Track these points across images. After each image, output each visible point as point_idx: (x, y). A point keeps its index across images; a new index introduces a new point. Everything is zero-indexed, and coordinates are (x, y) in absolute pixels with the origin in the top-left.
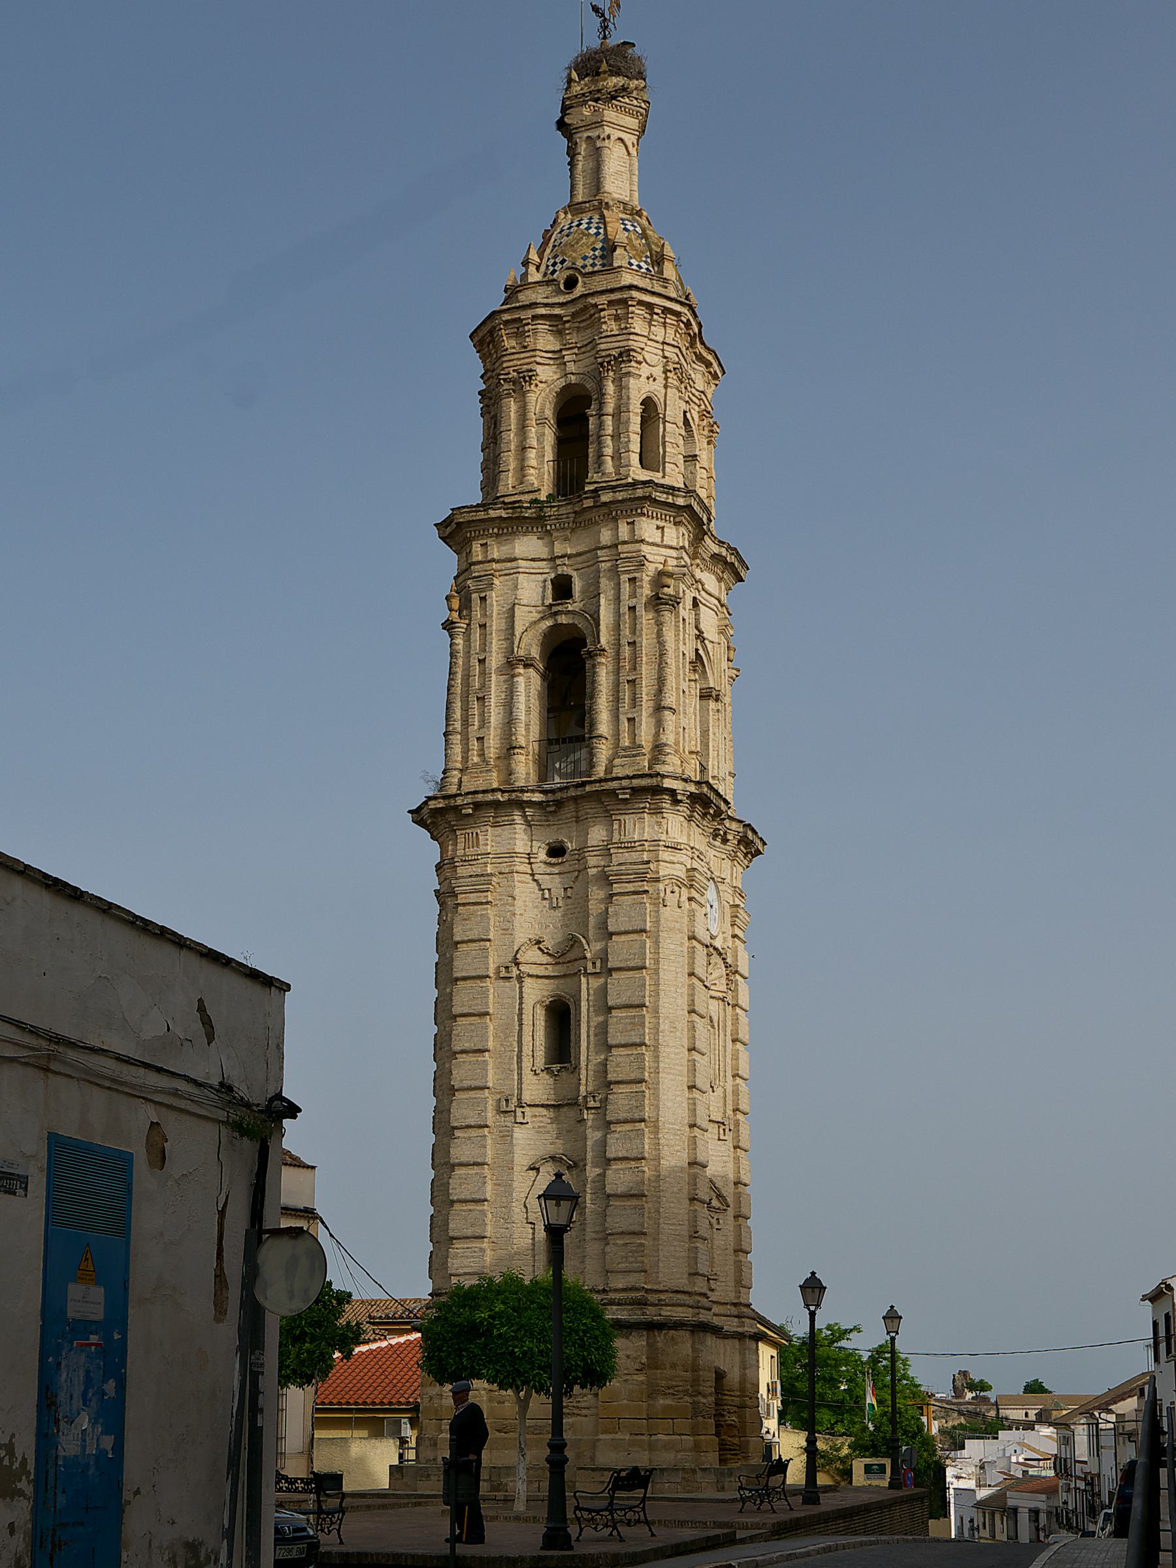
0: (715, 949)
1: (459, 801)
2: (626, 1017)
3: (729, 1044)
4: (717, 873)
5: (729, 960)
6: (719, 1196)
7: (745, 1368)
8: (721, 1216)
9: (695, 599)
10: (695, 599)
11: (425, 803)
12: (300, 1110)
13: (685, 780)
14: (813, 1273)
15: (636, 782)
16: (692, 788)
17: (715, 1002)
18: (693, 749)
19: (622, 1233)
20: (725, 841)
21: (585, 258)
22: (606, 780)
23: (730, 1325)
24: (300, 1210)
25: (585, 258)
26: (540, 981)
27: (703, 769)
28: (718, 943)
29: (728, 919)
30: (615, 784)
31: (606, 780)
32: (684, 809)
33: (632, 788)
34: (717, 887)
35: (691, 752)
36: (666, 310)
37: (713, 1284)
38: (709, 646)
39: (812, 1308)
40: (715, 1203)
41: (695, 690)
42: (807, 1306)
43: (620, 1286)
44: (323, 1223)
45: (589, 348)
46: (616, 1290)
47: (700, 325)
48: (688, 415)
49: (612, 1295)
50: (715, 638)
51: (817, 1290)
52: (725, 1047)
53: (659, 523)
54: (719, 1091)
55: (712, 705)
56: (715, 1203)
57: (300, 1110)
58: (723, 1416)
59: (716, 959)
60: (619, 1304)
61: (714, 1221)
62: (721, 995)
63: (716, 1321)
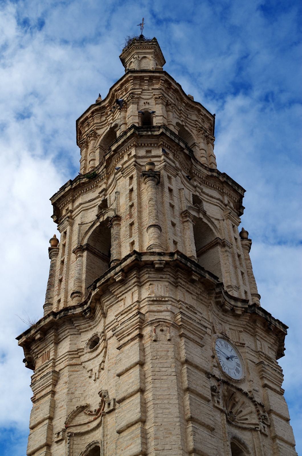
9: (195, 197)
16: (167, 258)
38: (216, 222)
62: (253, 427)
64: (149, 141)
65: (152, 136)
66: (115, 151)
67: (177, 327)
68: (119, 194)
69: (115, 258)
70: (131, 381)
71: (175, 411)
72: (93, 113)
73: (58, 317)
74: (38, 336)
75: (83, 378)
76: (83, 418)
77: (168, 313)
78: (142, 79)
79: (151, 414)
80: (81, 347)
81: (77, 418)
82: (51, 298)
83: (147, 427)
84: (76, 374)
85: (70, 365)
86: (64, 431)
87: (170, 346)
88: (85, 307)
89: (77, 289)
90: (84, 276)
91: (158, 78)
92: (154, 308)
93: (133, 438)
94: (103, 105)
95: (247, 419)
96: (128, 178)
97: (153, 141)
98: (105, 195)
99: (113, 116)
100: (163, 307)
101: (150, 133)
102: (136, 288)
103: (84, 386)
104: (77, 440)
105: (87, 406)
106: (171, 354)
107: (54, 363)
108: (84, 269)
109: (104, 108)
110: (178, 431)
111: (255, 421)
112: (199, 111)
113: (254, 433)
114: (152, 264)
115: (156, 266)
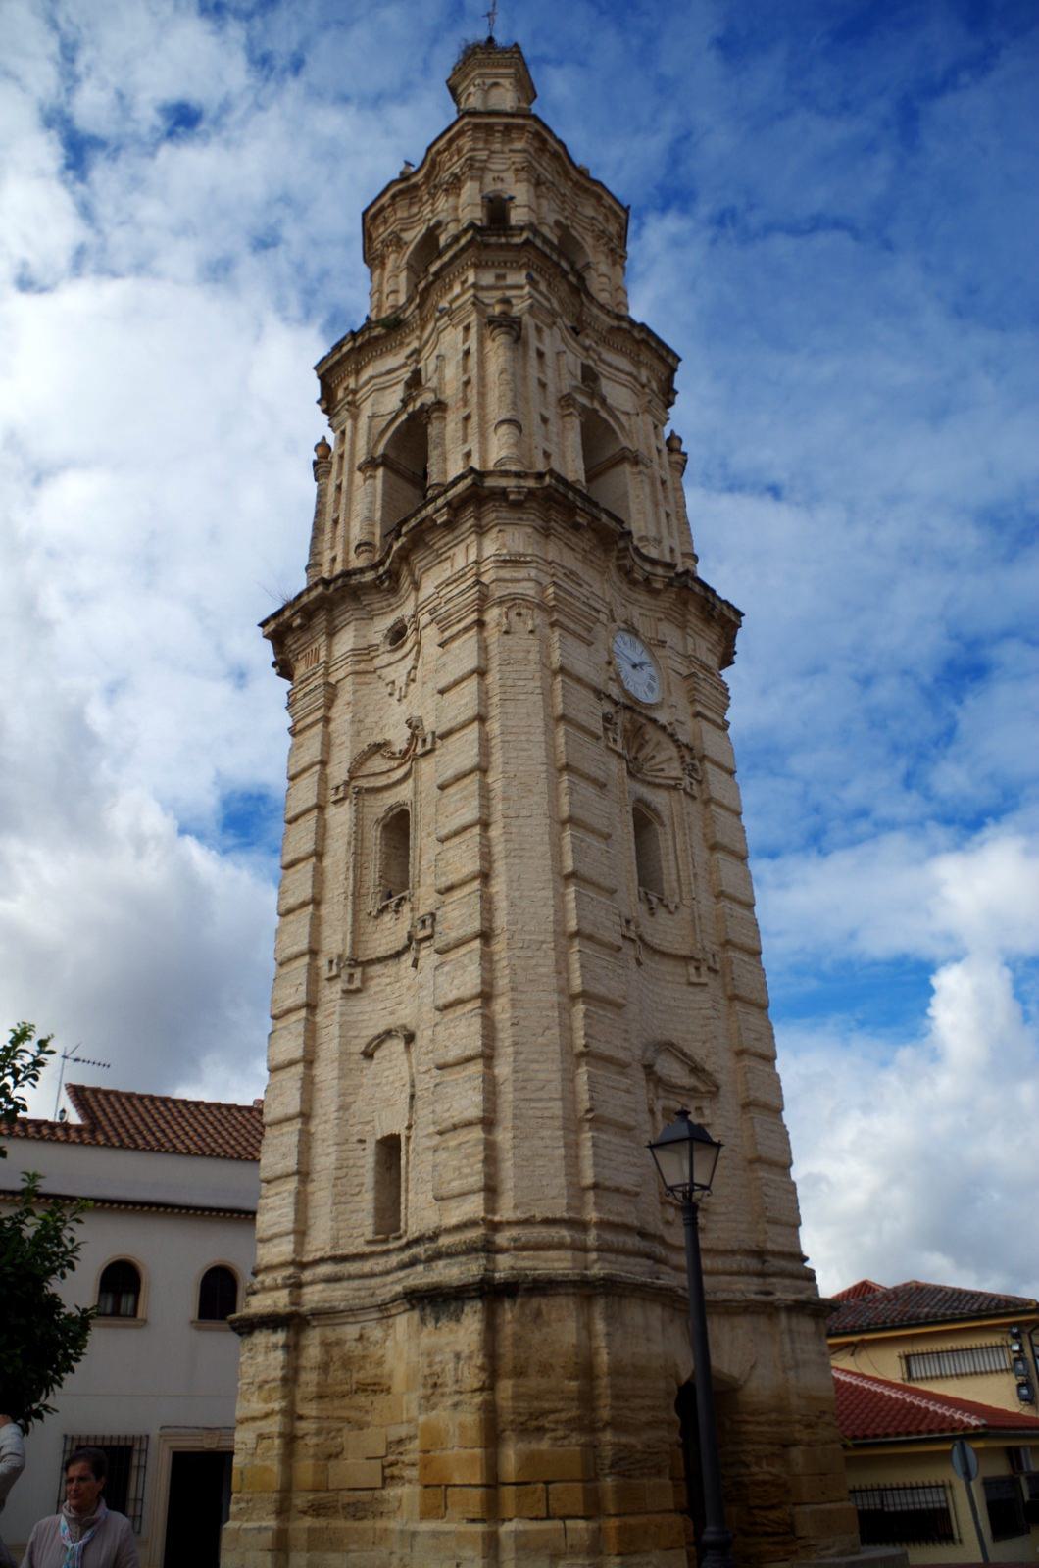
16: (531, 483)
38: (623, 418)
62: (673, 783)
64: (502, 256)
65: (509, 247)
66: (437, 274)
67: (542, 606)
70: (463, 702)
71: (539, 753)
72: (394, 197)
76: (379, 764)
77: (531, 584)
78: (489, 129)
83: (490, 780)
84: (365, 690)
85: (356, 673)
86: (347, 784)
90: (378, 515)
91: (521, 128)
92: (505, 574)
93: (465, 798)
94: (413, 180)
95: (662, 770)
96: (460, 328)
97: (510, 255)
98: (417, 361)
99: (433, 204)
100: (522, 574)
103: (381, 709)
105: (386, 744)
106: (534, 656)
109: (416, 187)
113: (674, 793)
114: (503, 493)
115: (512, 497)
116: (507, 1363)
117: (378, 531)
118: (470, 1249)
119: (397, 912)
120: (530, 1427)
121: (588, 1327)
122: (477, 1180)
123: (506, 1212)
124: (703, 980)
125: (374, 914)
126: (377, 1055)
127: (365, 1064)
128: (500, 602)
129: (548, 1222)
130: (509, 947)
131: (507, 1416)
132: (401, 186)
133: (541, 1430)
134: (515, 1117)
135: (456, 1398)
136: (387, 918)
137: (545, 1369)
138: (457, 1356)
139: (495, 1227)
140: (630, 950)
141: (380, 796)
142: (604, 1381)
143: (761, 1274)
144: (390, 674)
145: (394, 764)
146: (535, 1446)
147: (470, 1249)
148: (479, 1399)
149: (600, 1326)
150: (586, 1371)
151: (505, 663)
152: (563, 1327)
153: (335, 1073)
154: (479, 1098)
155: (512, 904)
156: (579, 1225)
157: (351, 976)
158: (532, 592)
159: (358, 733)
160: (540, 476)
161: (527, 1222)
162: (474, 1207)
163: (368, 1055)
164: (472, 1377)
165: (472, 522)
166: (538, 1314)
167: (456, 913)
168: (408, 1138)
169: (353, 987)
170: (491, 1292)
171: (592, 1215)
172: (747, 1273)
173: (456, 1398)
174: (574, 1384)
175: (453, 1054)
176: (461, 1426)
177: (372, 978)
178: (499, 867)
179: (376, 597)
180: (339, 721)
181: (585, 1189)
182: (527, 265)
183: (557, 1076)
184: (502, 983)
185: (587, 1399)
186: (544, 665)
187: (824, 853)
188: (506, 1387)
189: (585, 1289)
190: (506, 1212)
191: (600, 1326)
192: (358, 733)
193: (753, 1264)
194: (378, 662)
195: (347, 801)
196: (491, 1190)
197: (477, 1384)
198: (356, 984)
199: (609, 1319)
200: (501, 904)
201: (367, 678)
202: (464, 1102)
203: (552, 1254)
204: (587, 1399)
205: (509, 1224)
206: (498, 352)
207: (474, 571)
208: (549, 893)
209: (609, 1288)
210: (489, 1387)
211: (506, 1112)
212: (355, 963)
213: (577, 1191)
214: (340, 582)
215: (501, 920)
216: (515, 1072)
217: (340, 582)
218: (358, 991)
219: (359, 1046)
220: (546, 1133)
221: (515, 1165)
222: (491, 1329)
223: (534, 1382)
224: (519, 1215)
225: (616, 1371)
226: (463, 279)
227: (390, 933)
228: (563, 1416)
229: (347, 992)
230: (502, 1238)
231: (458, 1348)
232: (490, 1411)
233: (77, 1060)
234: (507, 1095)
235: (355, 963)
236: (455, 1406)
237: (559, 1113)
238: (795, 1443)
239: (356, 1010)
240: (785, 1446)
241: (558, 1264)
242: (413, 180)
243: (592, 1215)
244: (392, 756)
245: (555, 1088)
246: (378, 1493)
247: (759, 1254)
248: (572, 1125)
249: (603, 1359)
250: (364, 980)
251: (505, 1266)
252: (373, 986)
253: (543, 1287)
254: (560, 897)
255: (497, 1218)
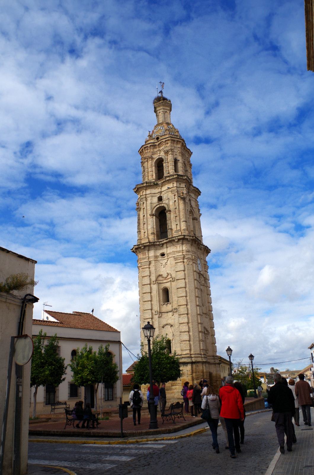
0: (201, 274)
1: (141, 246)
2: (181, 290)
3: (206, 296)
4: (200, 257)
5: (205, 276)
6: (207, 331)
7: (217, 371)
8: (208, 335)
9: (190, 199)
10: (190, 199)
11: (134, 247)
12: (39, 299)
13: (190, 236)
14: (229, 347)
15: (179, 237)
16: (191, 238)
17: (202, 286)
18: (192, 230)
19: (184, 341)
20: (201, 249)
21: (160, 133)
22: (172, 238)
23: (212, 361)
24: (117, 342)
25: (160, 133)
26: (285, 361)
27: (195, 234)
28: (202, 273)
29: (203, 267)
30: (174, 238)
31: (172, 238)
32: (190, 243)
33: (178, 239)
34: (200, 260)
35: (191, 231)
36: (178, 141)
37: (207, 352)
38: (194, 209)
39: (230, 355)
40: (206, 332)
41: (191, 217)
42: (228, 355)
43: (184, 353)
44: (122, 343)
45: (162, 150)
46: (184, 355)
47: (185, 144)
48: (185, 162)
49: (183, 356)
50: (195, 207)
51: (230, 351)
52: (205, 296)
53: (180, 183)
54: (205, 306)
55: (195, 221)
56: (206, 332)
57: (39, 299)
58: (212, 383)
59: (201, 276)
60: (184, 358)
61: (206, 337)
62: (203, 284)
63: (209, 361)
64: (181, 180)
65: (182, 179)
66: (168, 180)
67: (193, 260)
68: (169, 199)
69: (170, 228)
70: (181, 275)
71: (193, 286)
72: (150, 146)
73: (151, 244)
74: (143, 248)
75: (159, 265)
76: (160, 278)
77: (191, 255)
78: (174, 141)
79: (187, 286)
80: (158, 255)
81: (159, 278)
82: (140, 229)
83: (186, 289)
84: (156, 263)
85: (155, 260)
86: (155, 281)
87: (191, 266)
88: (160, 243)
89: (153, 232)
90: (155, 227)
91: (180, 142)
92: (187, 253)
93: (183, 292)
94: (155, 144)
95: (202, 282)
96: (173, 195)
97: (182, 180)
98: (161, 194)
99: (160, 152)
100: (189, 254)
101: (182, 178)
102: (181, 245)
103: (160, 268)
104: (160, 285)
105: (162, 275)
106: (192, 269)
107: (149, 258)
108: (155, 224)
109: (156, 145)
110: (194, 291)
111: (204, 283)
112: (188, 152)
113: (204, 286)
114: (187, 239)
115: (189, 240)
116: (194, 371)
117: (155, 230)
118: (188, 357)
119: (166, 305)
120: (197, 379)
121: (203, 367)
122: (189, 348)
123: (192, 353)
124: (207, 317)
125: (162, 305)
126: (165, 327)
127: (162, 328)
128: (187, 259)
129: (198, 354)
130: (191, 316)
131: (194, 378)
132: (153, 144)
133: (198, 379)
134: (193, 340)
135: (187, 376)
136: (164, 305)
137: (199, 372)
138: (187, 371)
139: (191, 354)
140: (204, 315)
141: (161, 284)
142: (205, 373)
143: (214, 359)
144: (161, 262)
145: (164, 279)
146: (198, 381)
147: (188, 357)
148: (191, 376)
149: (204, 367)
150: (203, 372)
151: (188, 270)
152: (200, 367)
153: (158, 329)
154: (188, 337)
155: (191, 310)
156: (201, 354)
157: (159, 314)
158: (191, 257)
159: (156, 272)
160: (193, 237)
161: (196, 354)
162: (188, 352)
163: (163, 327)
164: (190, 373)
165: (181, 242)
166: (198, 365)
167: (182, 310)
168: (172, 341)
169: (160, 316)
170: (192, 363)
171: (202, 353)
172: (212, 359)
173: (187, 376)
174: (202, 374)
175: (183, 331)
176: (189, 379)
177: (162, 315)
178: (189, 304)
179: (158, 247)
180: (151, 268)
181: (201, 350)
182: (185, 183)
183: (198, 335)
184: (190, 321)
185: (203, 375)
186: (193, 270)
187: (121, 218)
188: (194, 374)
189: (203, 363)
190: (192, 353)
191: (204, 367)
192: (156, 272)
193: (213, 358)
194: (158, 259)
195: (156, 284)
196: (190, 350)
197: (190, 374)
198: (160, 316)
199: (205, 366)
200: (189, 309)
201: (157, 261)
202: (186, 338)
203: (199, 358)
204: (203, 375)
205: (193, 354)
206: (181, 202)
207: (182, 252)
208: (196, 308)
209: (205, 362)
210: (192, 374)
211: (192, 340)
212: (160, 313)
213: (201, 350)
214: (152, 243)
215: (190, 312)
216: (193, 334)
217: (152, 243)
218: (161, 317)
219: (162, 325)
220: (197, 342)
221: (193, 347)
222: (192, 367)
223: (197, 374)
224: (194, 353)
225: (206, 372)
226: (173, 183)
227: (165, 308)
228: (201, 377)
229: (159, 317)
230: (193, 356)
231: (187, 370)
232: (192, 377)
233: (46, 305)
234: (192, 337)
235: (160, 313)
236: (187, 376)
237: (198, 340)
238: (217, 381)
239: (160, 320)
240: (216, 381)
241: (199, 359)
242: (155, 144)
243: (202, 353)
244: (163, 277)
245: (197, 336)
246: (171, 387)
247: (213, 356)
248: (200, 341)
249: (205, 371)
250: (161, 315)
251: (194, 360)
252: (163, 316)
253: (198, 362)
254: (197, 308)
255: (191, 353)
